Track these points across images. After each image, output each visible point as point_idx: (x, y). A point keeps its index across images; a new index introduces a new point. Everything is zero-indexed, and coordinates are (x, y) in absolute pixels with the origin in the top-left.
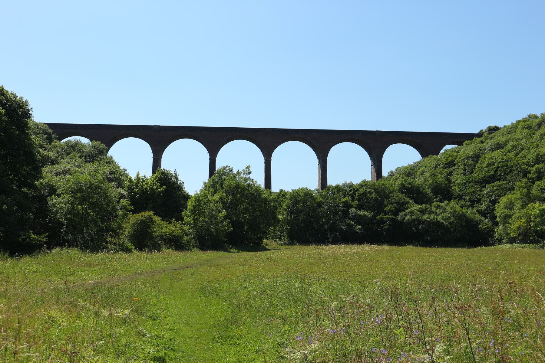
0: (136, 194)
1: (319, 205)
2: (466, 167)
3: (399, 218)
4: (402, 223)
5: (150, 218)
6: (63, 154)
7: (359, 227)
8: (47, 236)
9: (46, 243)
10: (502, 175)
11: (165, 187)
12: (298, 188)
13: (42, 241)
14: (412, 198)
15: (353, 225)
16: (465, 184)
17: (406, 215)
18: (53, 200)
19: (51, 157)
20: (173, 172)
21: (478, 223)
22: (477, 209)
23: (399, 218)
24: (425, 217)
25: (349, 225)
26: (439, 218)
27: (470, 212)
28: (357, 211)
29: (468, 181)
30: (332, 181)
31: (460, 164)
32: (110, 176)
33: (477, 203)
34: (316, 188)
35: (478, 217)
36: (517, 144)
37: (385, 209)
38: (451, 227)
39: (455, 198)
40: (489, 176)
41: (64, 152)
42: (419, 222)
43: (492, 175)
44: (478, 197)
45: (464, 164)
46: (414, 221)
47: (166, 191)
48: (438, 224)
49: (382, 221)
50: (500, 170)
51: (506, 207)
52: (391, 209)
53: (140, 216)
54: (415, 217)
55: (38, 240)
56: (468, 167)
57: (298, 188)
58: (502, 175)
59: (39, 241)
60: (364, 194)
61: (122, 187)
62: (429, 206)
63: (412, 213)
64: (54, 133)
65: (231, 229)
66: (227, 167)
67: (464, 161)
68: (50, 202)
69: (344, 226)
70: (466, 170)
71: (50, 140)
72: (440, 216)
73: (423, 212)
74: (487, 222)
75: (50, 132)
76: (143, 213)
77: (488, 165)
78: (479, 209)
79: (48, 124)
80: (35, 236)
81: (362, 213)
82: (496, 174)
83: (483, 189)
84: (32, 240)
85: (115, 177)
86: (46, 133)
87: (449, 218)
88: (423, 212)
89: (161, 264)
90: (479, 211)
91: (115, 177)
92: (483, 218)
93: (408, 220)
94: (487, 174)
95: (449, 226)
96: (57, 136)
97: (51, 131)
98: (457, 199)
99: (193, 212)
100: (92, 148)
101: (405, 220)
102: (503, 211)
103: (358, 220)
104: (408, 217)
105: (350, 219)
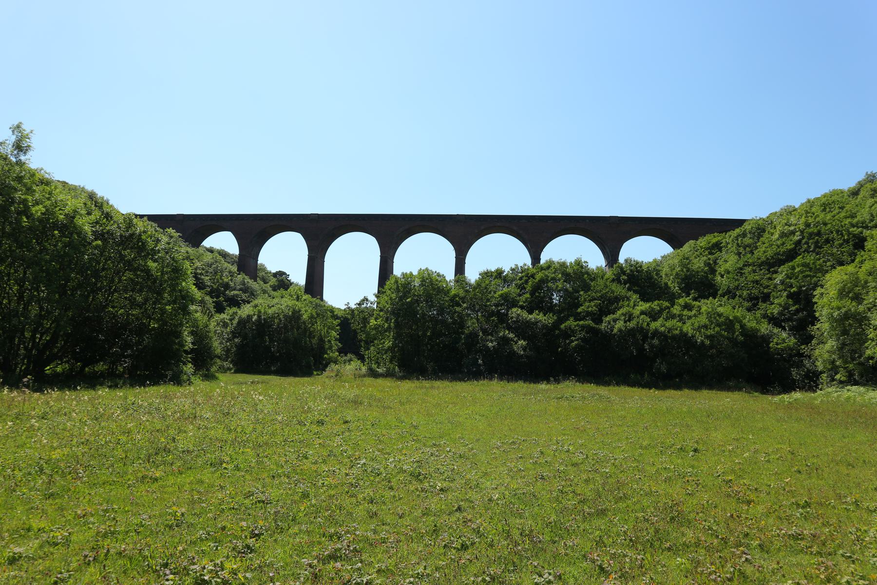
2: (741, 250)
3: (603, 326)
4: (606, 337)
7: (522, 342)
10: (811, 250)
12: (408, 272)
14: (635, 292)
16: (741, 269)
17: (615, 321)
21: (766, 339)
22: (764, 312)
23: (603, 326)
24: (654, 325)
25: (505, 341)
26: (688, 328)
27: (750, 321)
28: (525, 315)
29: (746, 265)
31: (729, 246)
33: (764, 301)
34: (24, 130)
35: (765, 328)
36: (830, 202)
37: (579, 310)
38: (711, 347)
39: (723, 295)
40: (784, 252)
42: (641, 333)
43: (790, 250)
44: (765, 291)
45: (738, 244)
46: (632, 332)
48: (685, 340)
49: (568, 334)
50: (807, 243)
51: (843, 293)
52: (590, 309)
54: (632, 324)
56: (745, 249)
57: (408, 272)
58: (811, 250)
60: (543, 281)
62: (667, 304)
63: (630, 317)
66: (42, 169)
67: (737, 240)
69: (492, 341)
70: (741, 253)
72: (689, 323)
73: (654, 316)
74: (783, 339)
77: (783, 235)
78: (768, 312)
79: (152, 218)
81: (532, 317)
82: (799, 250)
83: (774, 276)
87: (705, 327)
88: (654, 316)
90: (768, 316)
92: (776, 330)
93: (620, 330)
94: (782, 250)
95: (708, 342)
98: (726, 297)
101: (615, 331)
102: (835, 304)
103: (523, 329)
104: (620, 325)
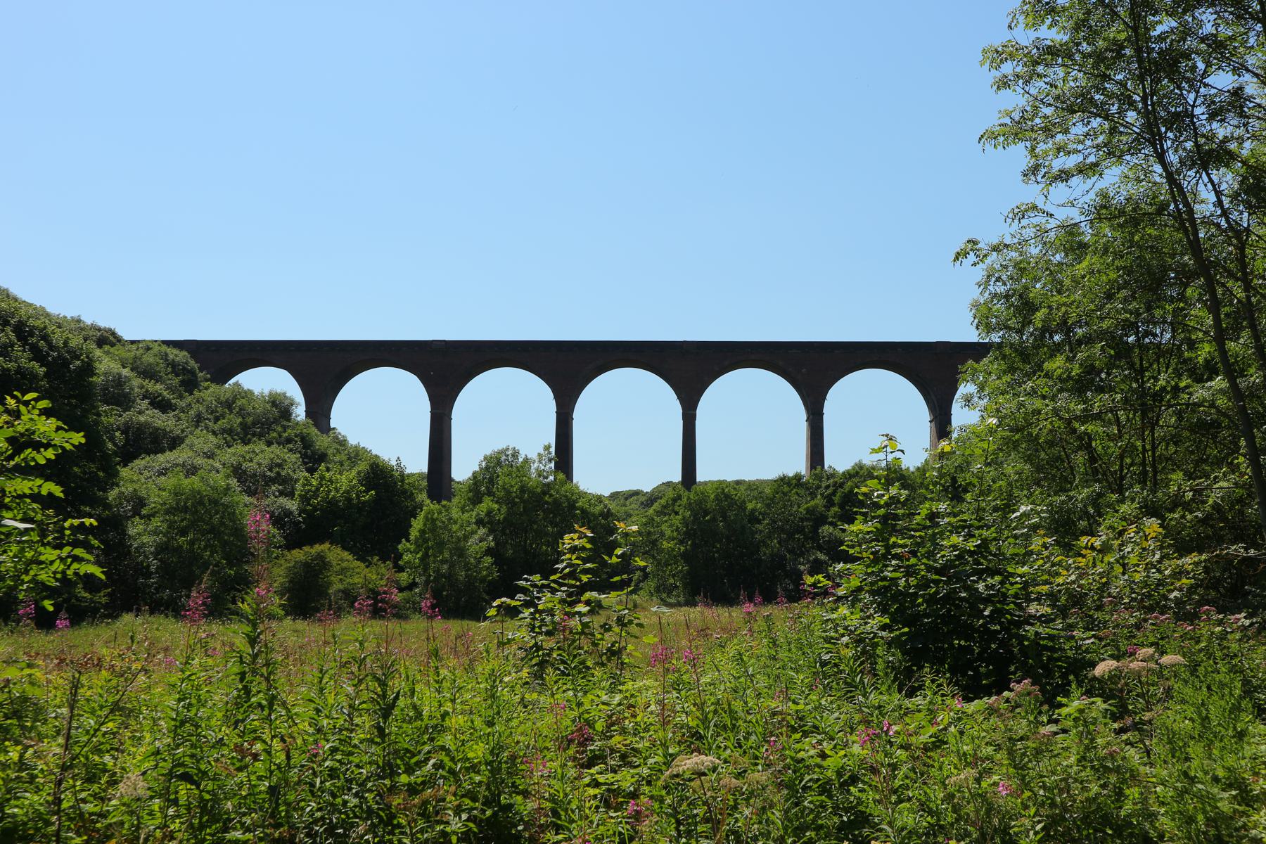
0: (315, 508)
1: (753, 518)
5: (321, 557)
6: (208, 419)
8: (108, 595)
9: (106, 606)
11: (373, 492)
13: (100, 603)
15: (825, 562)
18: (135, 528)
19: (171, 431)
20: (394, 463)
30: (704, 473)
32: (269, 473)
41: (212, 413)
47: (376, 501)
53: (298, 555)
55: (92, 601)
59: (93, 602)
61: (291, 495)
64: (201, 370)
65: (496, 574)
68: (132, 531)
71: (190, 384)
75: (193, 368)
76: (306, 548)
80: (87, 595)
84: (81, 601)
85: (278, 473)
86: (185, 370)
89: (712, 708)
91: (278, 473)
96: (209, 376)
97: (196, 366)
99: (422, 541)
100: (268, 406)
105: (820, 548)
